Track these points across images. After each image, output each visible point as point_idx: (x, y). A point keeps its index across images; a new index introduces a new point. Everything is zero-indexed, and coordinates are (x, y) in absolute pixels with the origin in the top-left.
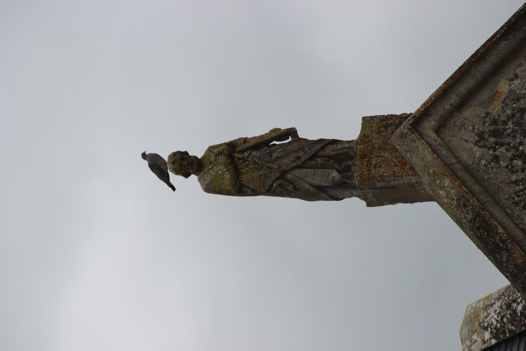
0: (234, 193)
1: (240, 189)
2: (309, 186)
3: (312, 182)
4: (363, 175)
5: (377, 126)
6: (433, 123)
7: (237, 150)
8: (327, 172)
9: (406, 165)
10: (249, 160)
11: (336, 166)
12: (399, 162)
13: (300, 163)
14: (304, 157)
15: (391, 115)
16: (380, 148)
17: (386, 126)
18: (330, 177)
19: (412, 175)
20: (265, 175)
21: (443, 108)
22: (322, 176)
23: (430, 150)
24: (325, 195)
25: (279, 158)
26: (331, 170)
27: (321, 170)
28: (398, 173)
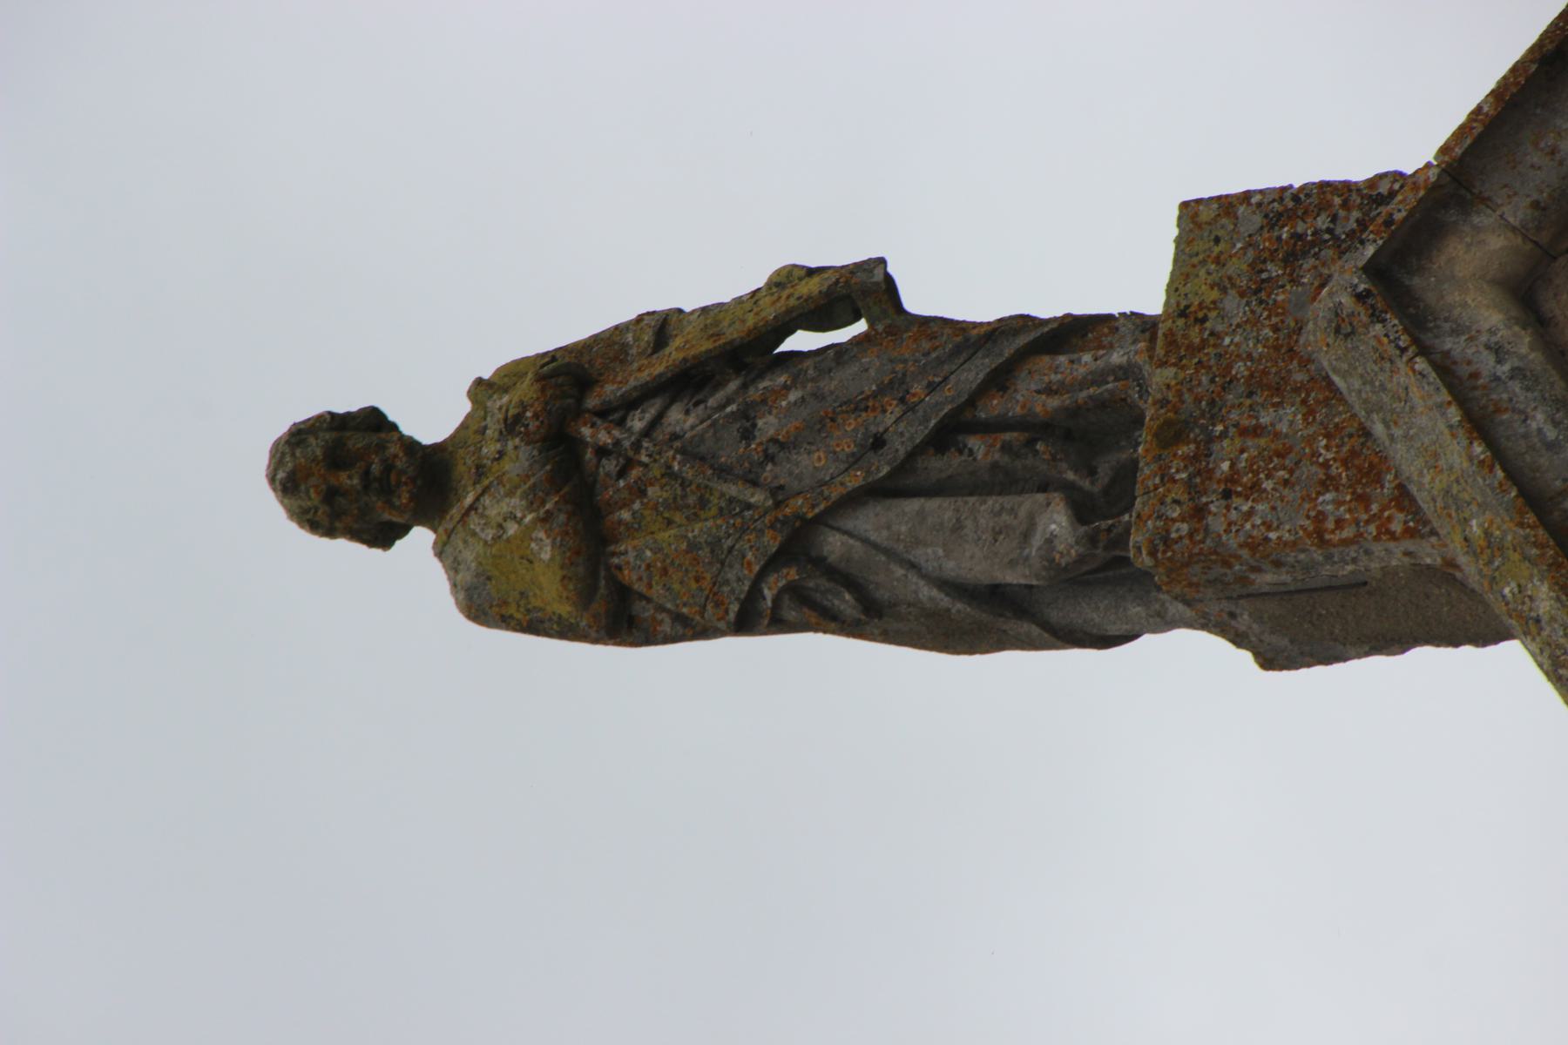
0: (594, 634)
1: (617, 613)
2: (935, 593)
3: (950, 568)
4: (1166, 541)
5: (1251, 254)
6: (1497, 243)
7: (592, 402)
8: (1022, 513)
9: (1379, 481)
10: (644, 459)
11: (1070, 476)
12: (1345, 463)
13: (885, 470)
14: (905, 432)
15: (1324, 186)
16: (1256, 383)
17: (1293, 254)
18: (1037, 541)
19: (1410, 533)
20: (714, 544)
21: (1553, 152)
22: (996, 534)
23: (1454, 415)
24: (1035, 630)
25: (782, 446)
26: (1041, 497)
27: (992, 502)
28: (1339, 523)
